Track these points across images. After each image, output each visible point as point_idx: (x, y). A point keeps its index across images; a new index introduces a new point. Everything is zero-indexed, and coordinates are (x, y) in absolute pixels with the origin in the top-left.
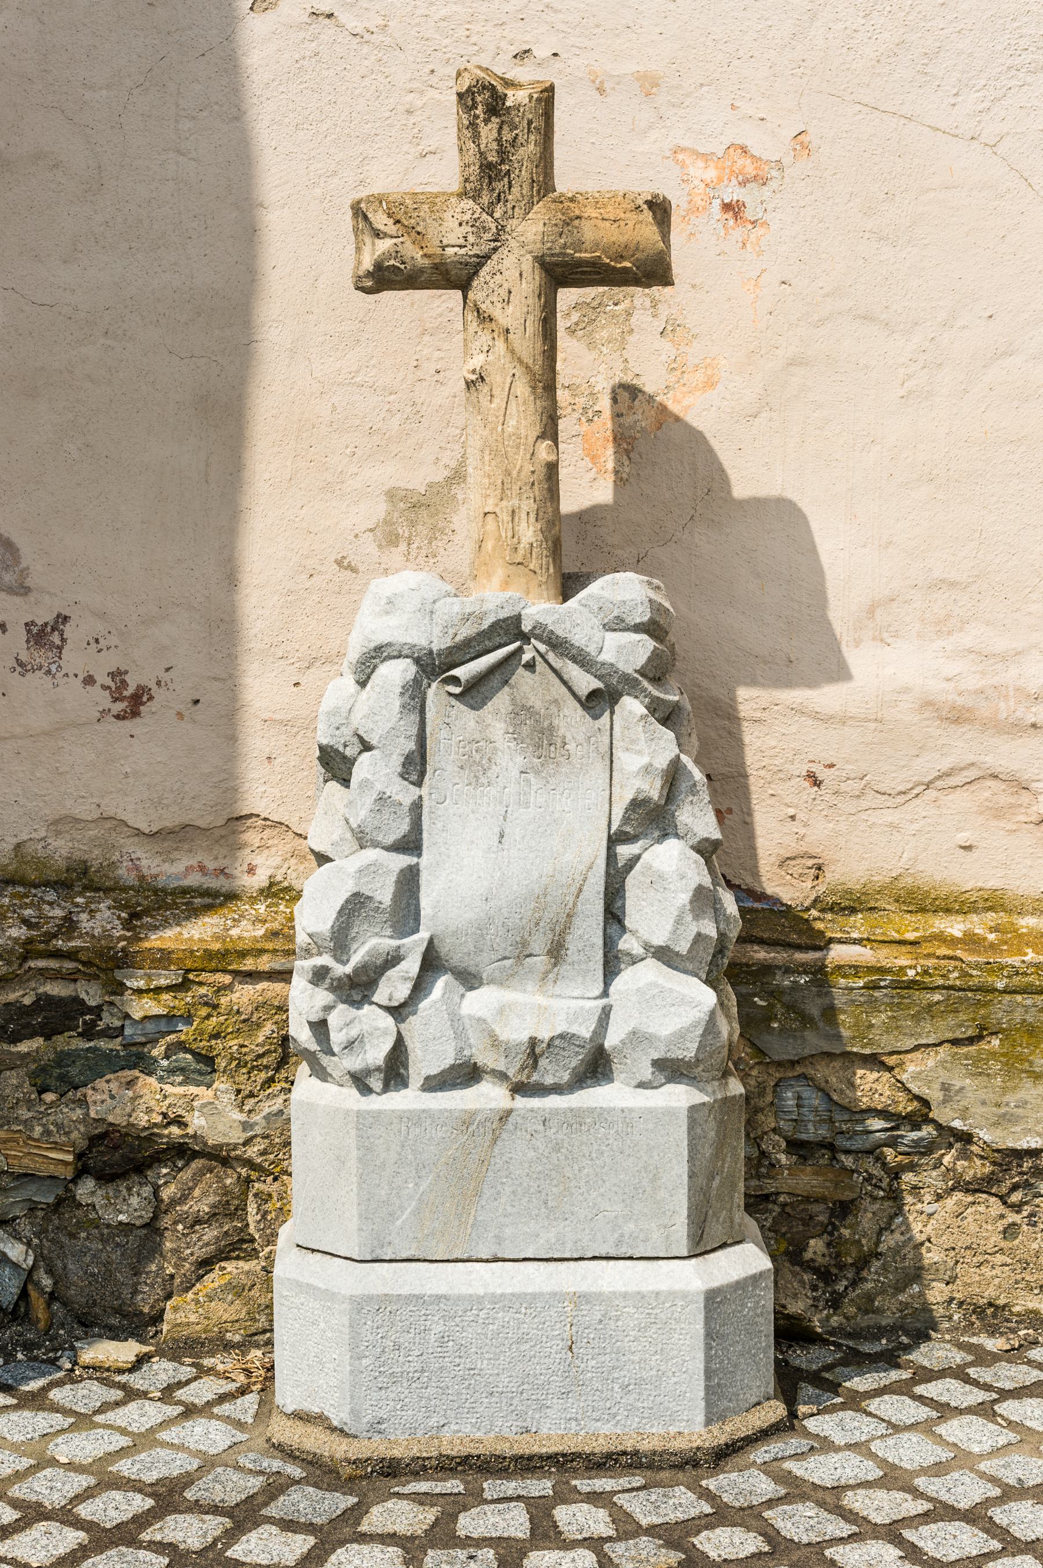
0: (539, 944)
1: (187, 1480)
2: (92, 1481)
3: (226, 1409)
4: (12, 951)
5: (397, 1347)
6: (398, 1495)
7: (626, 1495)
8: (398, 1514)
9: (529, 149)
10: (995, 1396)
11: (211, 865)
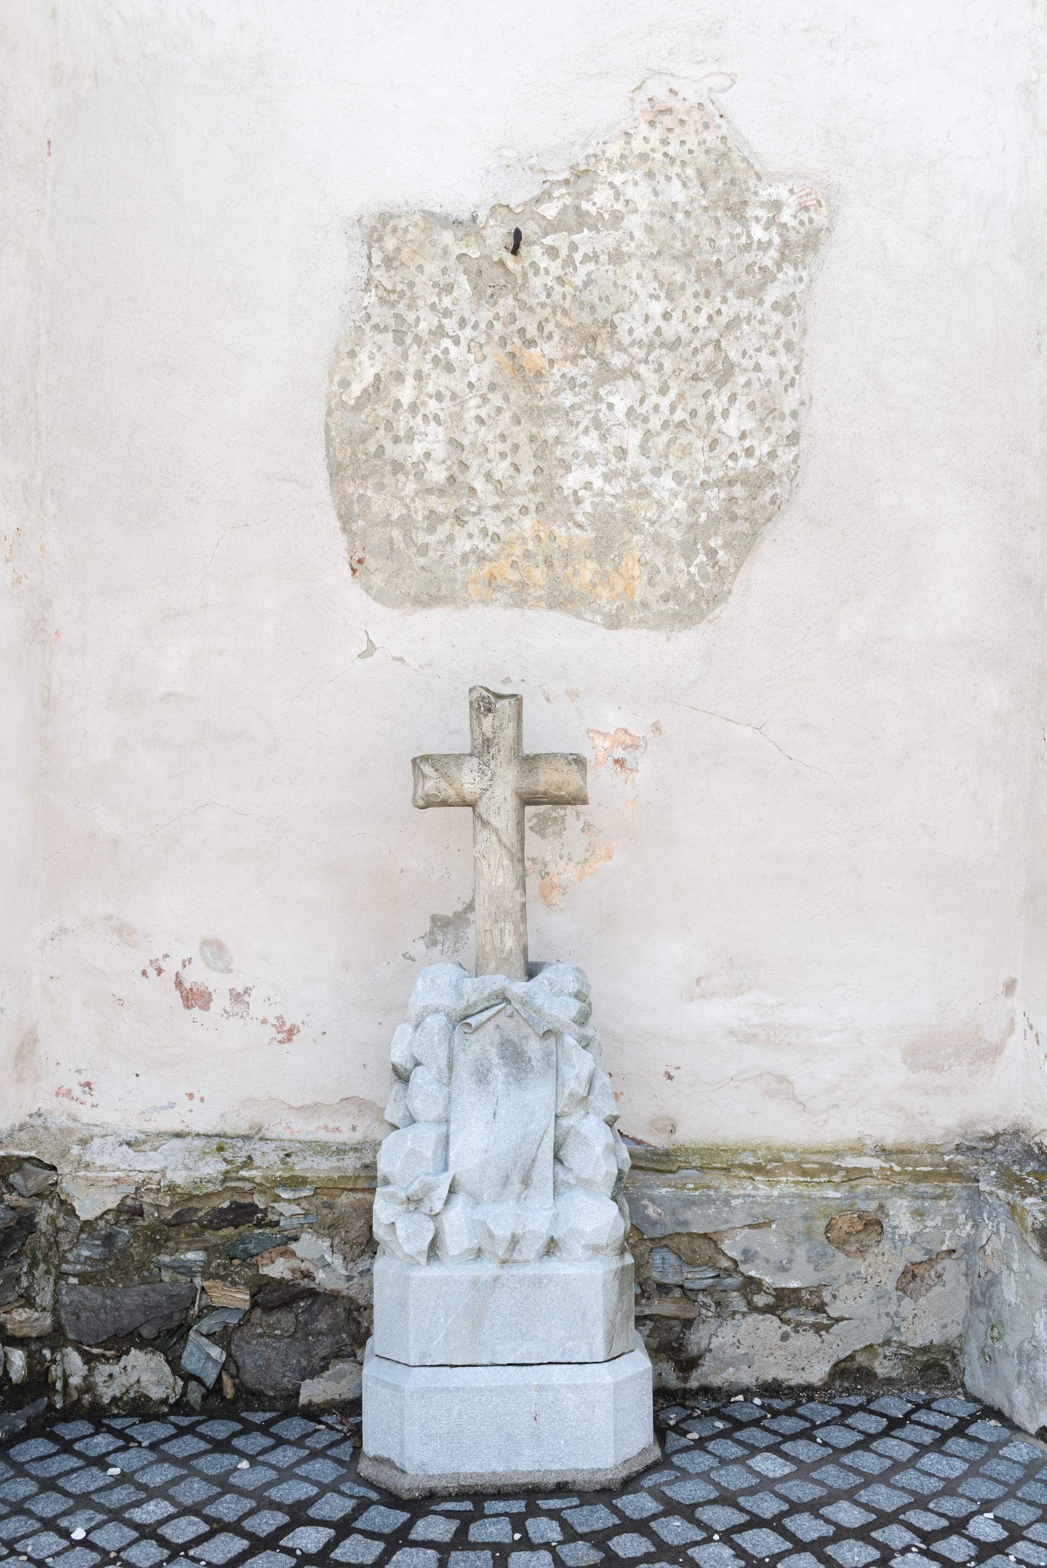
0: (516, 1178)
1: (310, 1501)
2: (254, 1504)
3: (333, 1452)
4: (216, 1178)
5: (434, 1418)
6: (435, 1513)
7: (569, 1511)
8: (435, 1527)
9: (510, 731)
10: (780, 1439)
11: (331, 1126)
